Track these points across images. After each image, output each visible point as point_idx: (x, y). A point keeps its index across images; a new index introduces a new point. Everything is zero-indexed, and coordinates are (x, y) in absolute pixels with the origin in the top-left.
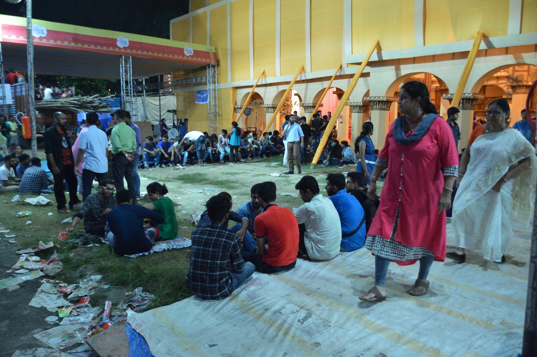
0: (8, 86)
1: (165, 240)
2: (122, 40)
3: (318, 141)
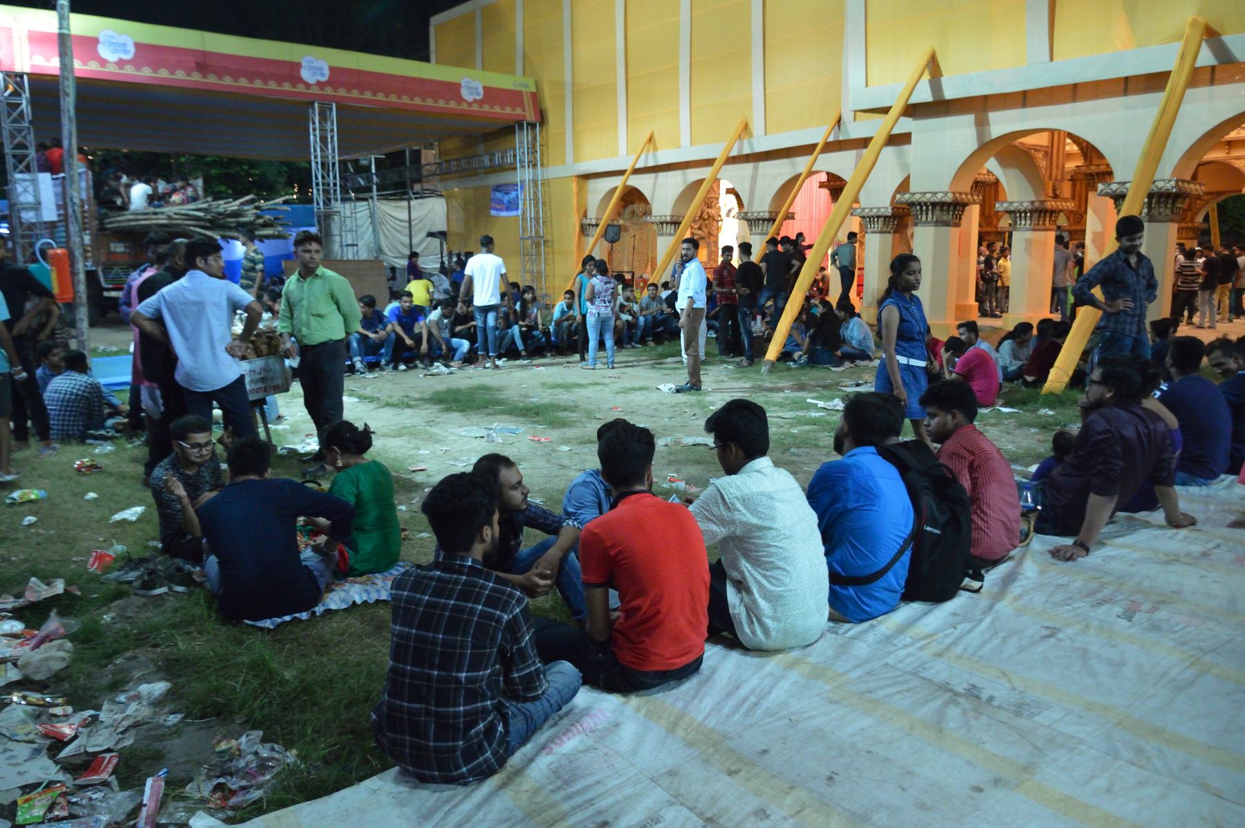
0: (45, 179)
1: (361, 575)
2: (313, 65)
3: (780, 305)
